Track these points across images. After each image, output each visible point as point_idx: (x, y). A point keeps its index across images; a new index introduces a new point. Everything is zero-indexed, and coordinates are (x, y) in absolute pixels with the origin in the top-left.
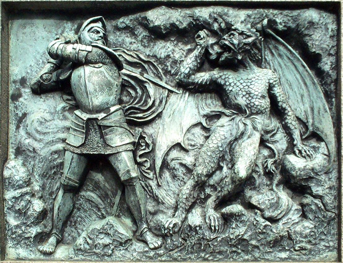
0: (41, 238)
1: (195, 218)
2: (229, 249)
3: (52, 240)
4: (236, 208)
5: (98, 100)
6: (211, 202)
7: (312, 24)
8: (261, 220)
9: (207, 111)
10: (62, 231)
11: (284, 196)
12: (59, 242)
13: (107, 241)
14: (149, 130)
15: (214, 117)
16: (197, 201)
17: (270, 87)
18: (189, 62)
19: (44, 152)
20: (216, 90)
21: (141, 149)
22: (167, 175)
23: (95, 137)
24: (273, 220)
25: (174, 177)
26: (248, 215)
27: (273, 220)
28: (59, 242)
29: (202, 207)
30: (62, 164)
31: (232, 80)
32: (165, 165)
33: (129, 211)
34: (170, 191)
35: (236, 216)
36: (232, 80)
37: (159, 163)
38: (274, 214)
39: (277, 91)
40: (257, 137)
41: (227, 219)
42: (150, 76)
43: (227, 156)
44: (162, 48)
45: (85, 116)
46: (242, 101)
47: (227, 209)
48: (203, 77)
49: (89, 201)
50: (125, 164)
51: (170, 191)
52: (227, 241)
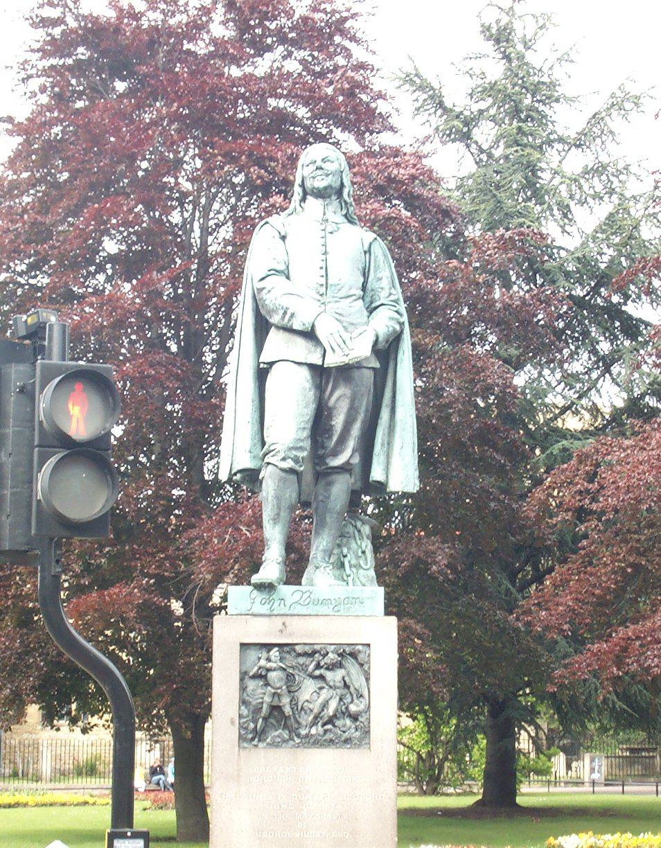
0: (253, 739)
1: (313, 731)
2: (232, 98)
3: (256, 740)
4: (329, 727)
5: (278, 685)
6: (320, 724)
7: (359, 651)
8: (339, 732)
9: (319, 686)
10: (260, 736)
11: (348, 722)
12: (259, 741)
13: (279, 740)
14: (296, 694)
15: (321, 688)
16: (314, 723)
17: (343, 678)
18: (311, 667)
19: (254, 703)
20: (322, 677)
21: (294, 702)
22: (303, 712)
23: (276, 698)
24: (344, 732)
25: (306, 713)
26: (334, 729)
27: (344, 732)
28: (259, 741)
29: (412, 202)
30: (262, 708)
31: (329, 675)
32: (302, 708)
33: (286, 727)
34: (306, 719)
35: (330, 730)
36: (329, 675)
37: (299, 708)
38: (344, 729)
39: (346, 679)
40: (338, 698)
41: (326, 731)
42: (297, 671)
43: (325, 705)
44: (302, 660)
45: (273, 691)
46: (331, 684)
47: (326, 727)
48: (317, 673)
49: (271, 723)
50: (287, 710)
51: (306, 719)
52: (325, 740)
